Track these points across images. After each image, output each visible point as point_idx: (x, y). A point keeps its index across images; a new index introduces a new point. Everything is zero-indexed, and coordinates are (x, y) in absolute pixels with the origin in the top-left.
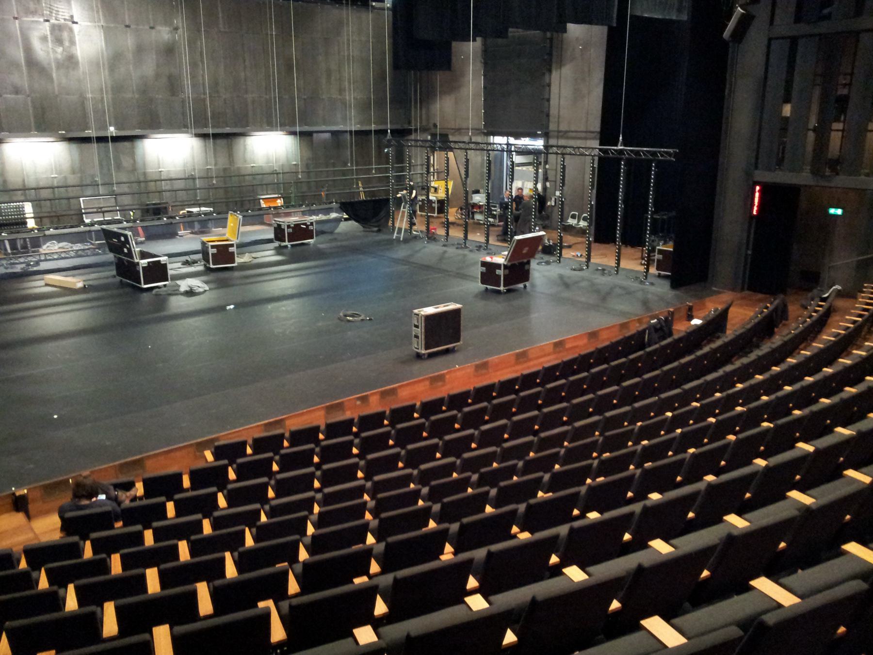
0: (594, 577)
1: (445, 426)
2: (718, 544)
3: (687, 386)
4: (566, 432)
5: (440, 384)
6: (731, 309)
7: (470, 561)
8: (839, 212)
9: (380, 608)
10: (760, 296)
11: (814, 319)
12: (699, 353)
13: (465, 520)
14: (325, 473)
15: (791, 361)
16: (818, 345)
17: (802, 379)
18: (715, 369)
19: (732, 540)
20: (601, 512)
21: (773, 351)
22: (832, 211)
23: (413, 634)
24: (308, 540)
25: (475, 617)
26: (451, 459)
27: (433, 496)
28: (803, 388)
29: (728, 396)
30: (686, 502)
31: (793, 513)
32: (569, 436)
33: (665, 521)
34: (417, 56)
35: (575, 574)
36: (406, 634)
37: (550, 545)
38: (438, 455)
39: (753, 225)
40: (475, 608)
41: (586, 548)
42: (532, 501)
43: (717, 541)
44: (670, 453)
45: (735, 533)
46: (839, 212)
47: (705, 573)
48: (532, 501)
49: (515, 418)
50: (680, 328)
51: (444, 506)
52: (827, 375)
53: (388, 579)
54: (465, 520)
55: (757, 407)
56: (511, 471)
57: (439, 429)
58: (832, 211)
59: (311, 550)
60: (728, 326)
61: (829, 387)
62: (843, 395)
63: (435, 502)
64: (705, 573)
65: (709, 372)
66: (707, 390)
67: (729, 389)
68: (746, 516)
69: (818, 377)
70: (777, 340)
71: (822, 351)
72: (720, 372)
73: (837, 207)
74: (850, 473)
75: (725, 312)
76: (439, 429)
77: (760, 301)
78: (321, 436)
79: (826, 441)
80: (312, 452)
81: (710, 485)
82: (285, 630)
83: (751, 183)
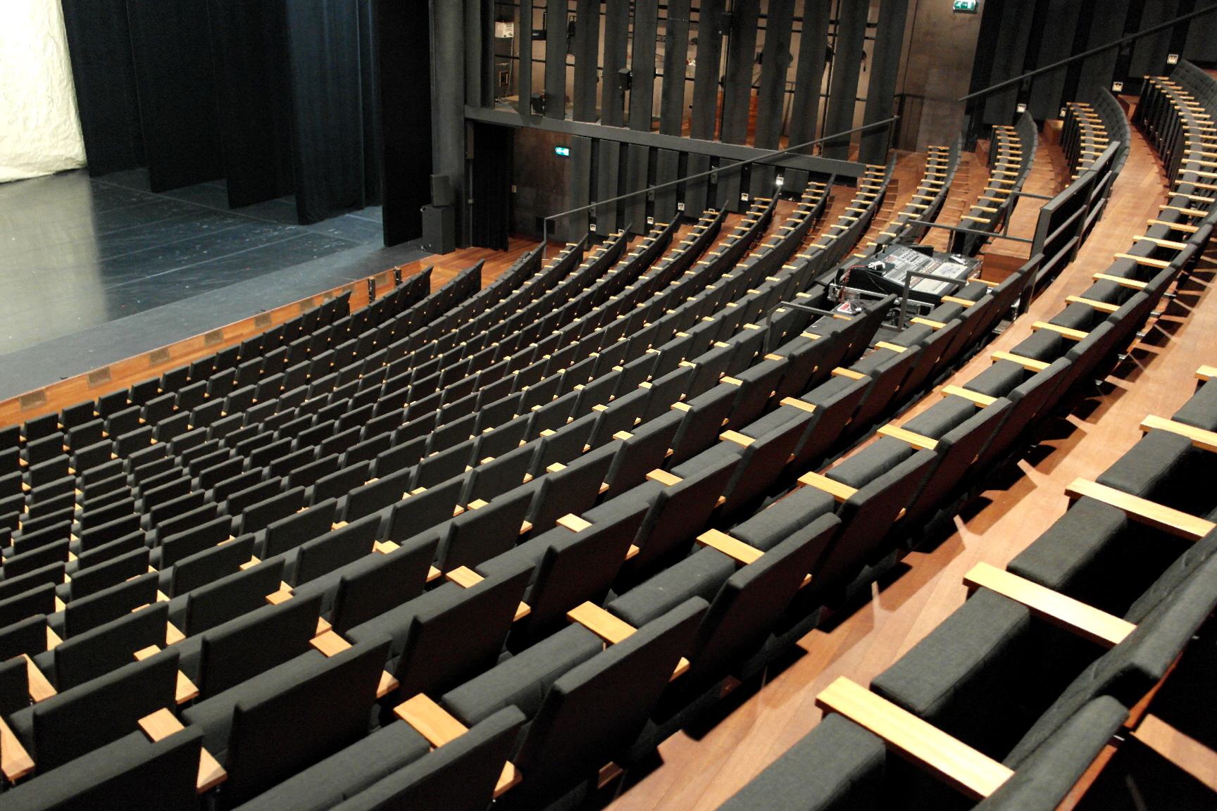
0: (490, 578)
1: (194, 398)
2: (645, 510)
3: (450, 313)
4: (334, 378)
5: (38, 403)
7: (281, 565)
8: (566, 152)
9: (185, 687)
13: (272, 526)
14: (32, 450)
15: (574, 274)
19: (664, 503)
20: (487, 499)
22: (559, 151)
23: (245, 707)
24: (47, 658)
25: (332, 666)
26: (202, 429)
27: (219, 496)
28: (546, 300)
30: (599, 468)
31: (735, 457)
32: (338, 381)
33: (575, 491)
35: (465, 577)
36: (231, 711)
37: (425, 555)
38: (190, 427)
40: (330, 653)
41: (472, 545)
42: (399, 504)
43: (647, 505)
45: (670, 493)
46: (566, 152)
47: (633, 550)
48: (399, 504)
49: (242, 366)
50: (1103, 200)
51: (247, 516)
53: (195, 645)
54: (272, 526)
56: (364, 474)
57: (190, 400)
58: (559, 151)
59: (58, 674)
61: (600, 296)
62: (686, 305)
63: (207, 489)
64: (633, 550)
69: (667, 291)
73: (563, 147)
76: (190, 400)
78: (22, 438)
80: (17, 454)
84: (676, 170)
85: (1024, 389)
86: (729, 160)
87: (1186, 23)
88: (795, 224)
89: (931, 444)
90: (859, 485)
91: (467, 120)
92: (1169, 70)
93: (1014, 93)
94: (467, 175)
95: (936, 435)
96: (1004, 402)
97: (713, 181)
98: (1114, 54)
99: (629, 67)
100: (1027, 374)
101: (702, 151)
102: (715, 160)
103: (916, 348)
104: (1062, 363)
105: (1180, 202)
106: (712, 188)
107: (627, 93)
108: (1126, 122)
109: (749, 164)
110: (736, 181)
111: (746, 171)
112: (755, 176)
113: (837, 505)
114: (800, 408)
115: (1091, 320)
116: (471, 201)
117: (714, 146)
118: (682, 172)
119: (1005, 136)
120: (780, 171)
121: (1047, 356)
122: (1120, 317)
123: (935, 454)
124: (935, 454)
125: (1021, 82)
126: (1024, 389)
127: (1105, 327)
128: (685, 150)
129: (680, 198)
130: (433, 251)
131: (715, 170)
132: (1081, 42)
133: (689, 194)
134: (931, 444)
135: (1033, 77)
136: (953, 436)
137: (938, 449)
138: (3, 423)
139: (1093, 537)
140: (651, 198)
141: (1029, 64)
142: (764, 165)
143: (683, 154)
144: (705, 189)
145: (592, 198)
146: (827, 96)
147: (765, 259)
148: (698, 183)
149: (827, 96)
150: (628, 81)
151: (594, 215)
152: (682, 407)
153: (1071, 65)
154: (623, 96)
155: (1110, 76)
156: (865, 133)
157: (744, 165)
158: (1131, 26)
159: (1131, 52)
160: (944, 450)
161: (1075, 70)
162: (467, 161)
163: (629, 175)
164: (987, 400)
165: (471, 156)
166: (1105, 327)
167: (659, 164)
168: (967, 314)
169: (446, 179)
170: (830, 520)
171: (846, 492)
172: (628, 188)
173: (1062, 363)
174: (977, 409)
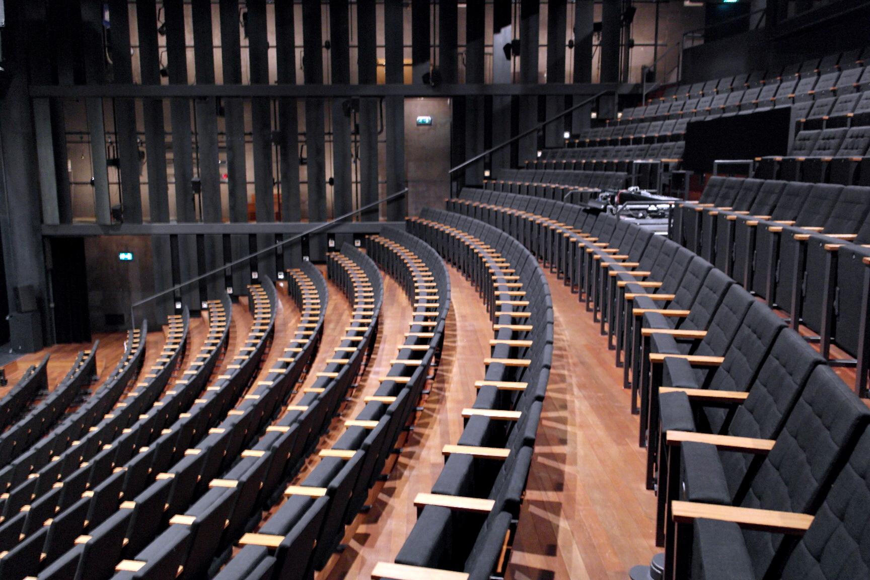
6: (49, 364)
8: (129, 256)
10: (74, 346)
11: (131, 361)
12: (22, 423)
16: (133, 394)
17: (138, 419)
18: (44, 433)
21: (89, 412)
22: (123, 256)
29: (68, 456)
34: (658, 3)
39: (50, 279)
44: (22, 536)
46: (129, 256)
52: (160, 408)
55: (101, 460)
58: (123, 256)
60: (49, 382)
62: (90, 435)
65: (38, 439)
66: (42, 458)
67: (66, 449)
68: (139, 556)
70: (92, 401)
71: (148, 389)
72: (32, 451)
73: (126, 252)
74: (215, 483)
75: (43, 371)
77: (75, 351)
79: (181, 466)
81: (89, 547)
82: (457, 25)
83: (40, 238)
84: (247, 248)
85: (368, 440)
86: (290, 235)
87: (570, 114)
88: (164, 364)
89: (322, 492)
90: (284, 533)
91: (44, 237)
92: (331, 250)
93: (482, 164)
94: (47, 284)
95: (324, 485)
96: (361, 453)
97: (279, 252)
98: (535, 135)
99: (196, 176)
100: (367, 431)
101: (268, 231)
102: (279, 236)
103: (295, 425)
104: (385, 418)
105: (421, 309)
106: (279, 257)
107: (197, 196)
108: (324, 280)
109: (307, 236)
110: (298, 249)
111: (305, 242)
112: (313, 244)
113: (270, 550)
114: (225, 484)
115: (396, 389)
116: (52, 305)
117: (277, 226)
118: (253, 248)
119: (260, 296)
120: (332, 236)
121: (376, 418)
122: (411, 384)
123: (328, 498)
124: (328, 498)
125: (484, 157)
126: (368, 440)
127: (404, 392)
128: (253, 232)
129: (254, 268)
130: (25, 351)
131: (279, 244)
132: (515, 131)
133: (261, 265)
134: (322, 492)
135: (491, 154)
136: (335, 483)
137: (327, 494)
138: (2, 399)
139: (435, 528)
140: (228, 273)
141: (488, 146)
142: (318, 234)
143: (253, 236)
144: (274, 259)
145: (176, 280)
146: (357, 182)
147: (141, 396)
148: (268, 255)
149: (357, 182)
150: (197, 186)
151: (178, 295)
152: (129, 506)
153: (512, 144)
154: (193, 199)
155: (535, 147)
156: (389, 202)
157: (302, 237)
158: (542, 117)
159: (544, 132)
160: (331, 493)
161: (515, 146)
162: (47, 272)
163: (207, 256)
164: (350, 454)
165: (50, 266)
166: (404, 392)
167: (233, 245)
168: (321, 396)
169: (30, 288)
170: (270, 560)
171: (276, 541)
172: (182, 277)
173: (385, 418)
174: (344, 461)
